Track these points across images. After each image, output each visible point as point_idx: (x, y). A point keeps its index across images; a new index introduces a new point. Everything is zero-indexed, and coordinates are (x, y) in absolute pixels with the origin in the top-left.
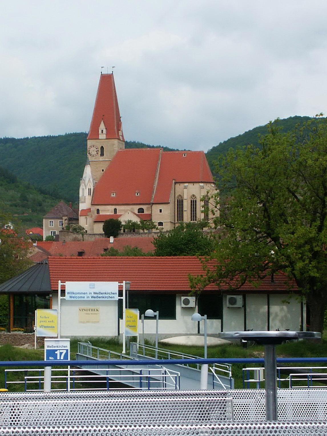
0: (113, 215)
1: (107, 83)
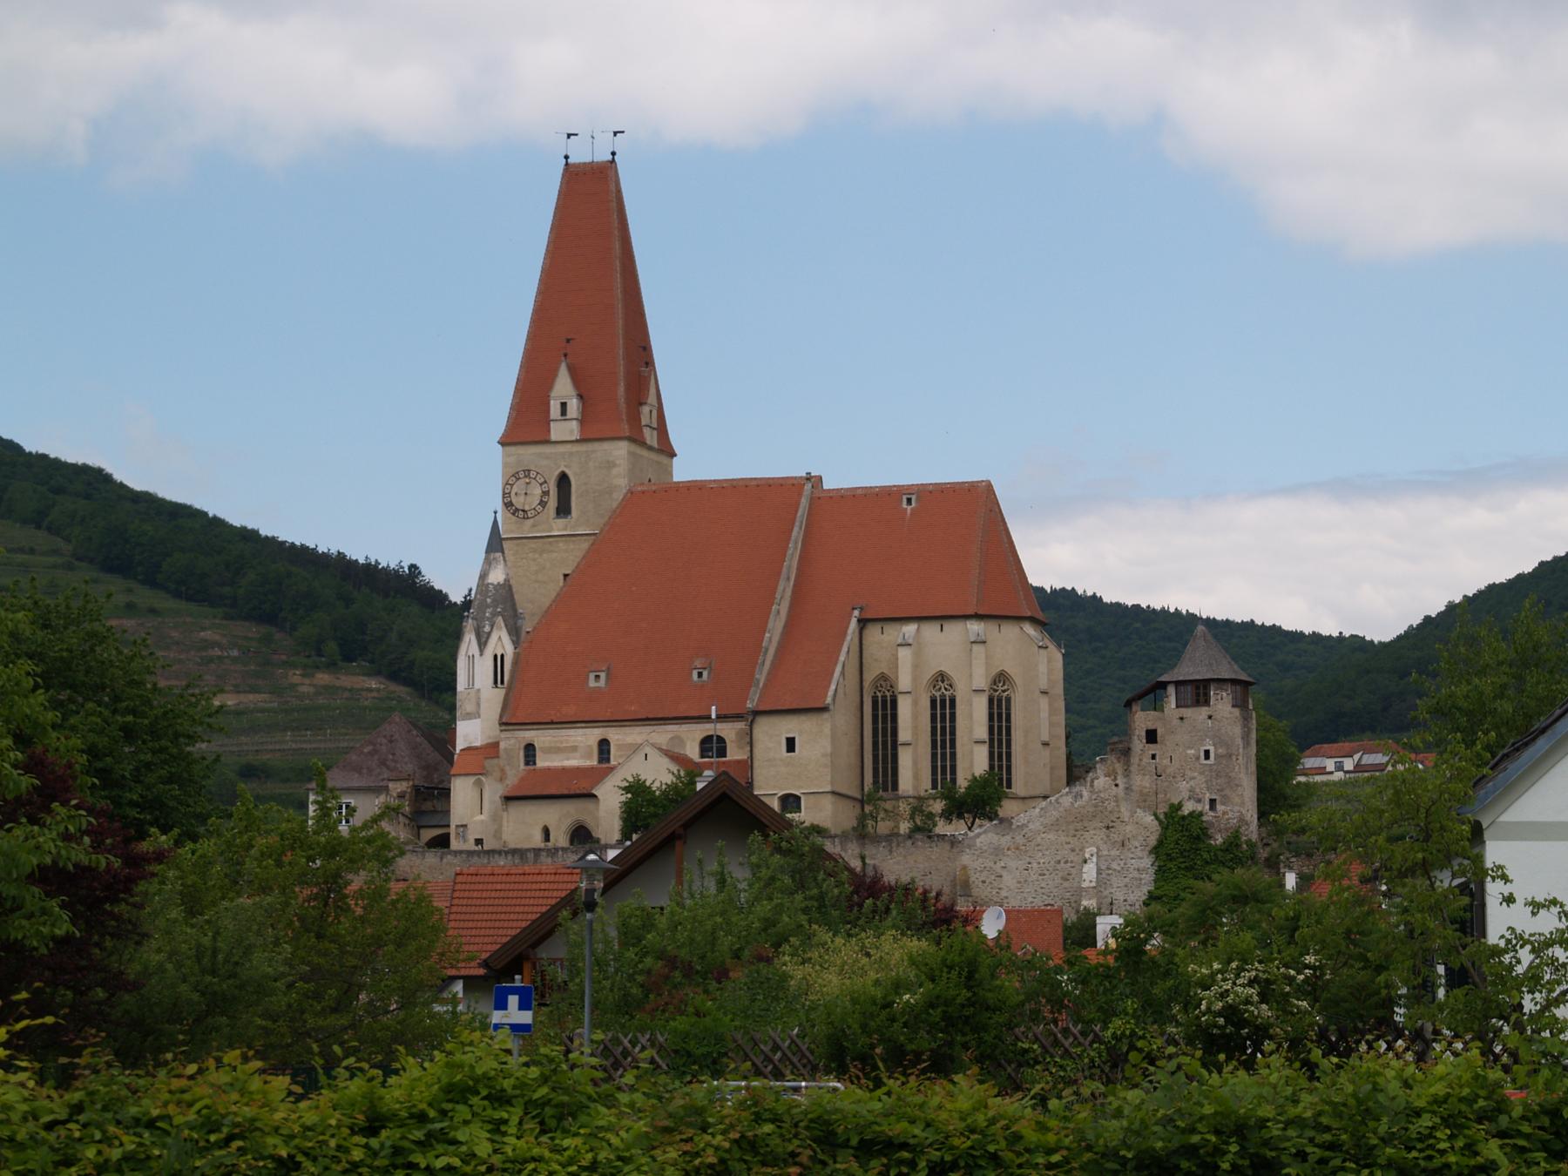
0: (592, 768)
1: (590, 202)
